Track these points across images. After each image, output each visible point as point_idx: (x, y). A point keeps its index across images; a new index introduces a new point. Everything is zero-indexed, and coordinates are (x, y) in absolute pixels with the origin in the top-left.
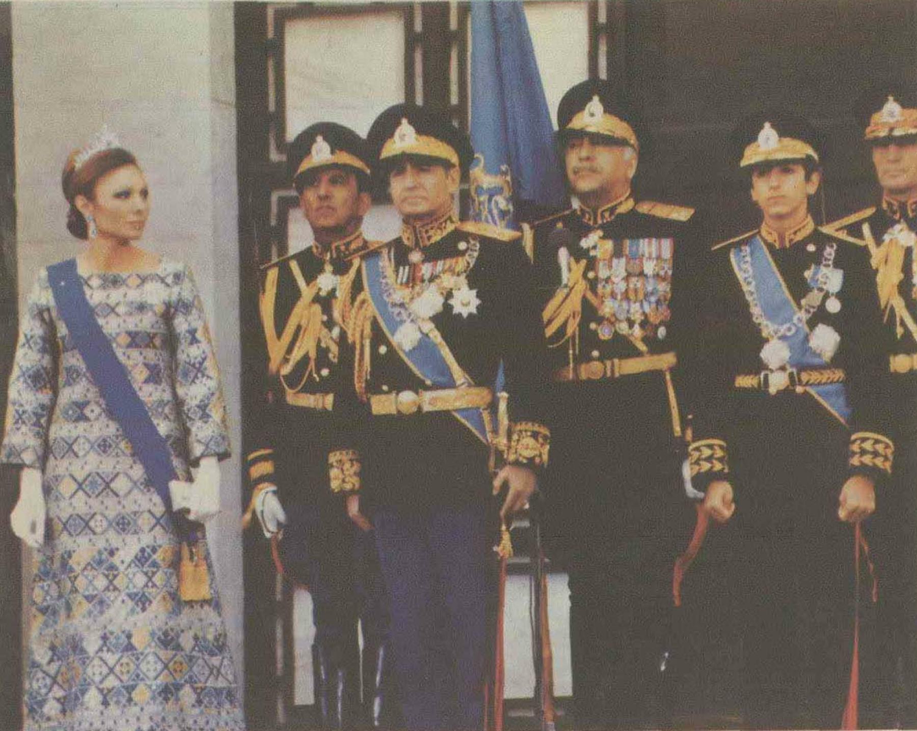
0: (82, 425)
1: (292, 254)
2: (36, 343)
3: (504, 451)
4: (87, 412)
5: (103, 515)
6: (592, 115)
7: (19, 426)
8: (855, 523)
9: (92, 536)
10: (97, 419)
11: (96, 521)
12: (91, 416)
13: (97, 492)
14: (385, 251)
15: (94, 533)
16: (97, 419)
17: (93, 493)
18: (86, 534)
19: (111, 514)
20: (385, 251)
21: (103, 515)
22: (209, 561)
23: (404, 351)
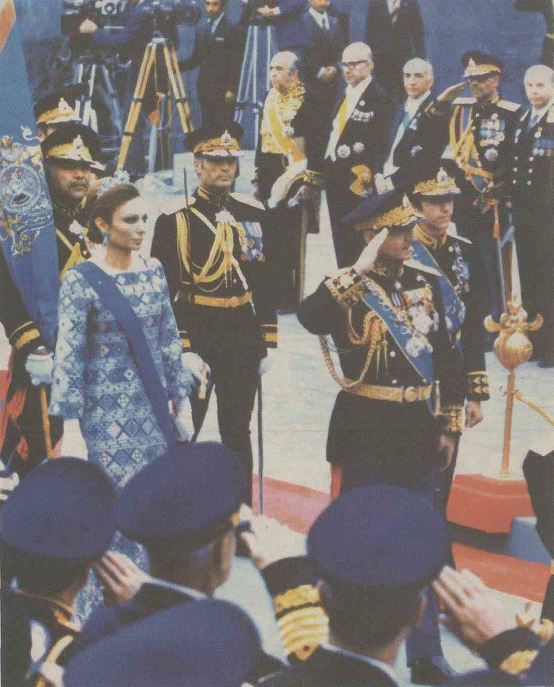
0: (123, 385)
1: (233, 197)
2: (82, 328)
3: (124, 169)
4: (126, 375)
5: (139, 449)
6: (65, 109)
7: (73, 389)
8: (426, 347)
9: (135, 464)
10: (133, 379)
11: (121, 399)
12: (129, 377)
13: (135, 433)
14: (80, 119)
15: (135, 462)
16: (133, 379)
17: (132, 434)
18: (130, 463)
19: (144, 447)
20: (80, 119)
21: (139, 449)
22: (169, 385)
23: (410, 357)
